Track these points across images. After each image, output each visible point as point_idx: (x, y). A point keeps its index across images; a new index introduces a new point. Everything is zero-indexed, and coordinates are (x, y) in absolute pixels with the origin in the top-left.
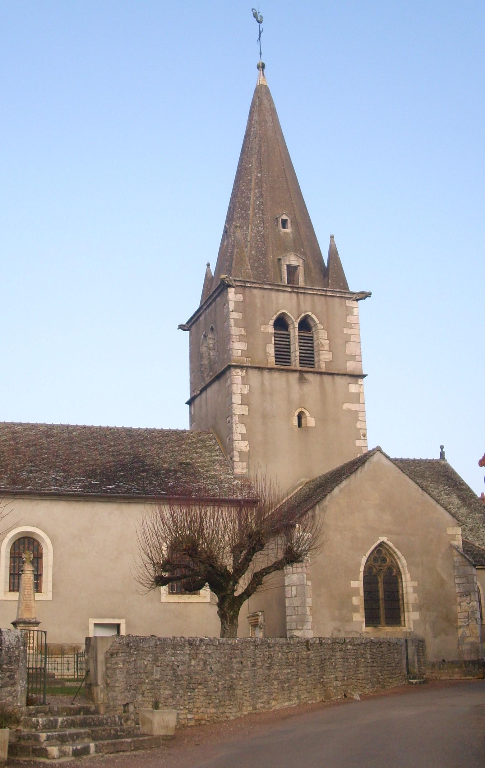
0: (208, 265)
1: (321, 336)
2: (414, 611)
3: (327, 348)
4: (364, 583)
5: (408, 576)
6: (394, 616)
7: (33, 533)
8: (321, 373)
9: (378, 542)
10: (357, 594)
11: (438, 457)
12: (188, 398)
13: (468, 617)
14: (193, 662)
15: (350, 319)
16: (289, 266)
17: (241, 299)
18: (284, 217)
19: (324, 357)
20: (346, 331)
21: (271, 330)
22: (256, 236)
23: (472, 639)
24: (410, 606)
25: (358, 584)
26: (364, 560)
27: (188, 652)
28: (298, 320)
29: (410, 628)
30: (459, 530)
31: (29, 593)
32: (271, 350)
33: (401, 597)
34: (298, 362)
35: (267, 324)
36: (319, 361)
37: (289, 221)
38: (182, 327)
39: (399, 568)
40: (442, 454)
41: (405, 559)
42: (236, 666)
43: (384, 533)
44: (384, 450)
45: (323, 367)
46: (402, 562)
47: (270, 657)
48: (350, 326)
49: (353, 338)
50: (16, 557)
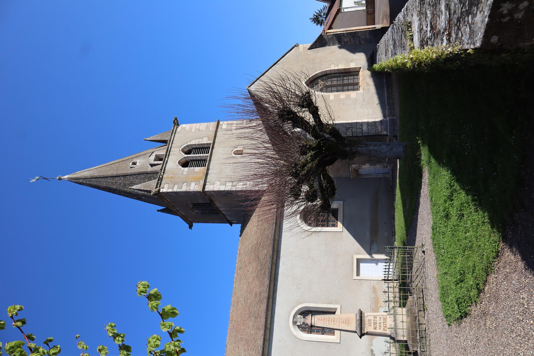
0: (158, 211)
6: (353, 73)
12: (228, 225)
16: (155, 160)
18: (131, 163)
20: (193, 131)
21: (186, 169)
31: (333, 320)
32: (197, 169)
38: (191, 227)
45: (211, 142)
50: (311, 329)
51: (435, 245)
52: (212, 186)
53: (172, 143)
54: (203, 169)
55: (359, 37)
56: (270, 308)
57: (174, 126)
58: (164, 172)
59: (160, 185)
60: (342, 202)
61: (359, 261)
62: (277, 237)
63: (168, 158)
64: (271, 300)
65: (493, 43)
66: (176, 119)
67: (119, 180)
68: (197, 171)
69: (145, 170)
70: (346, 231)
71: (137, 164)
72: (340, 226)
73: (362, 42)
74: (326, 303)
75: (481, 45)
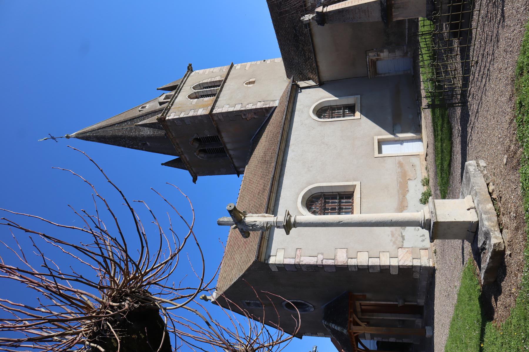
45: (223, 79)
51: (453, 324)
52: (221, 109)
53: (184, 84)
54: (213, 98)
56: (275, 191)
57: (188, 72)
58: (172, 105)
59: (167, 114)
60: (359, 96)
61: (381, 143)
62: (286, 129)
63: (178, 94)
64: (276, 184)
66: (190, 65)
67: (126, 126)
69: (153, 110)
70: (364, 118)
72: (358, 114)
74: (343, 181)
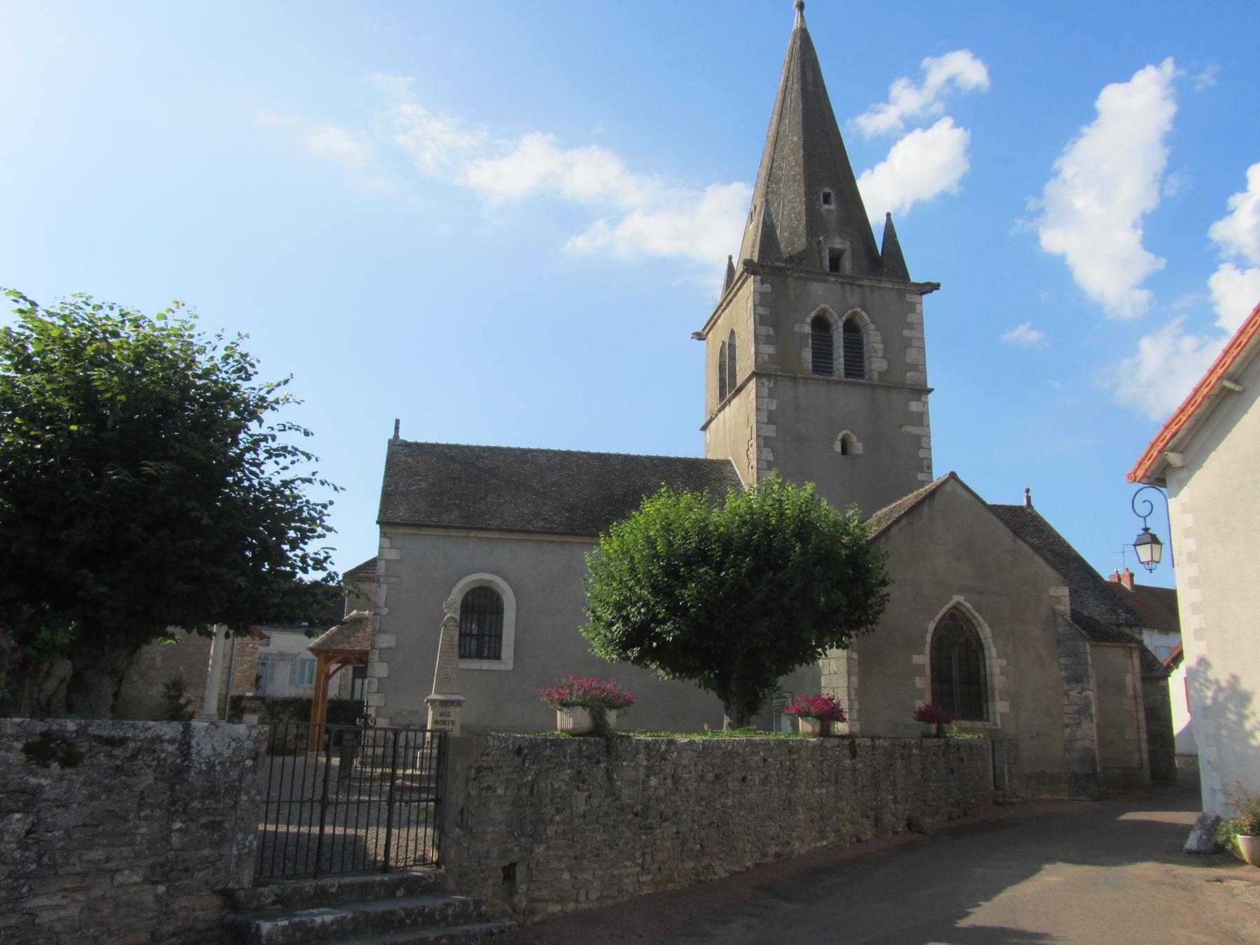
0: (730, 258)
1: (873, 340)
2: (1002, 699)
3: (880, 354)
4: (931, 657)
5: (994, 651)
7: (491, 582)
8: (873, 387)
9: (952, 603)
10: (923, 674)
11: (1024, 503)
13: (1079, 712)
14: (653, 781)
15: (911, 318)
16: (831, 250)
17: (770, 290)
18: (827, 190)
19: (876, 365)
20: (906, 333)
21: (807, 329)
22: (789, 214)
23: (1086, 744)
24: (997, 692)
25: (923, 659)
26: (931, 626)
27: (645, 763)
28: (844, 318)
29: (995, 724)
30: (1065, 591)
32: (807, 355)
33: (982, 681)
34: (842, 372)
35: (803, 322)
36: (870, 371)
37: (833, 195)
39: (979, 639)
40: (1028, 499)
41: (991, 627)
42: (734, 785)
43: (960, 591)
44: (960, 476)
46: (985, 631)
47: (793, 770)
48: (911, 326)
49: (915, 343)
55: (1079, 724)
65: (948, 722)
68: (803, 354)
71: (826, 206)
73: (1067, 731)
75: (955, 47)
